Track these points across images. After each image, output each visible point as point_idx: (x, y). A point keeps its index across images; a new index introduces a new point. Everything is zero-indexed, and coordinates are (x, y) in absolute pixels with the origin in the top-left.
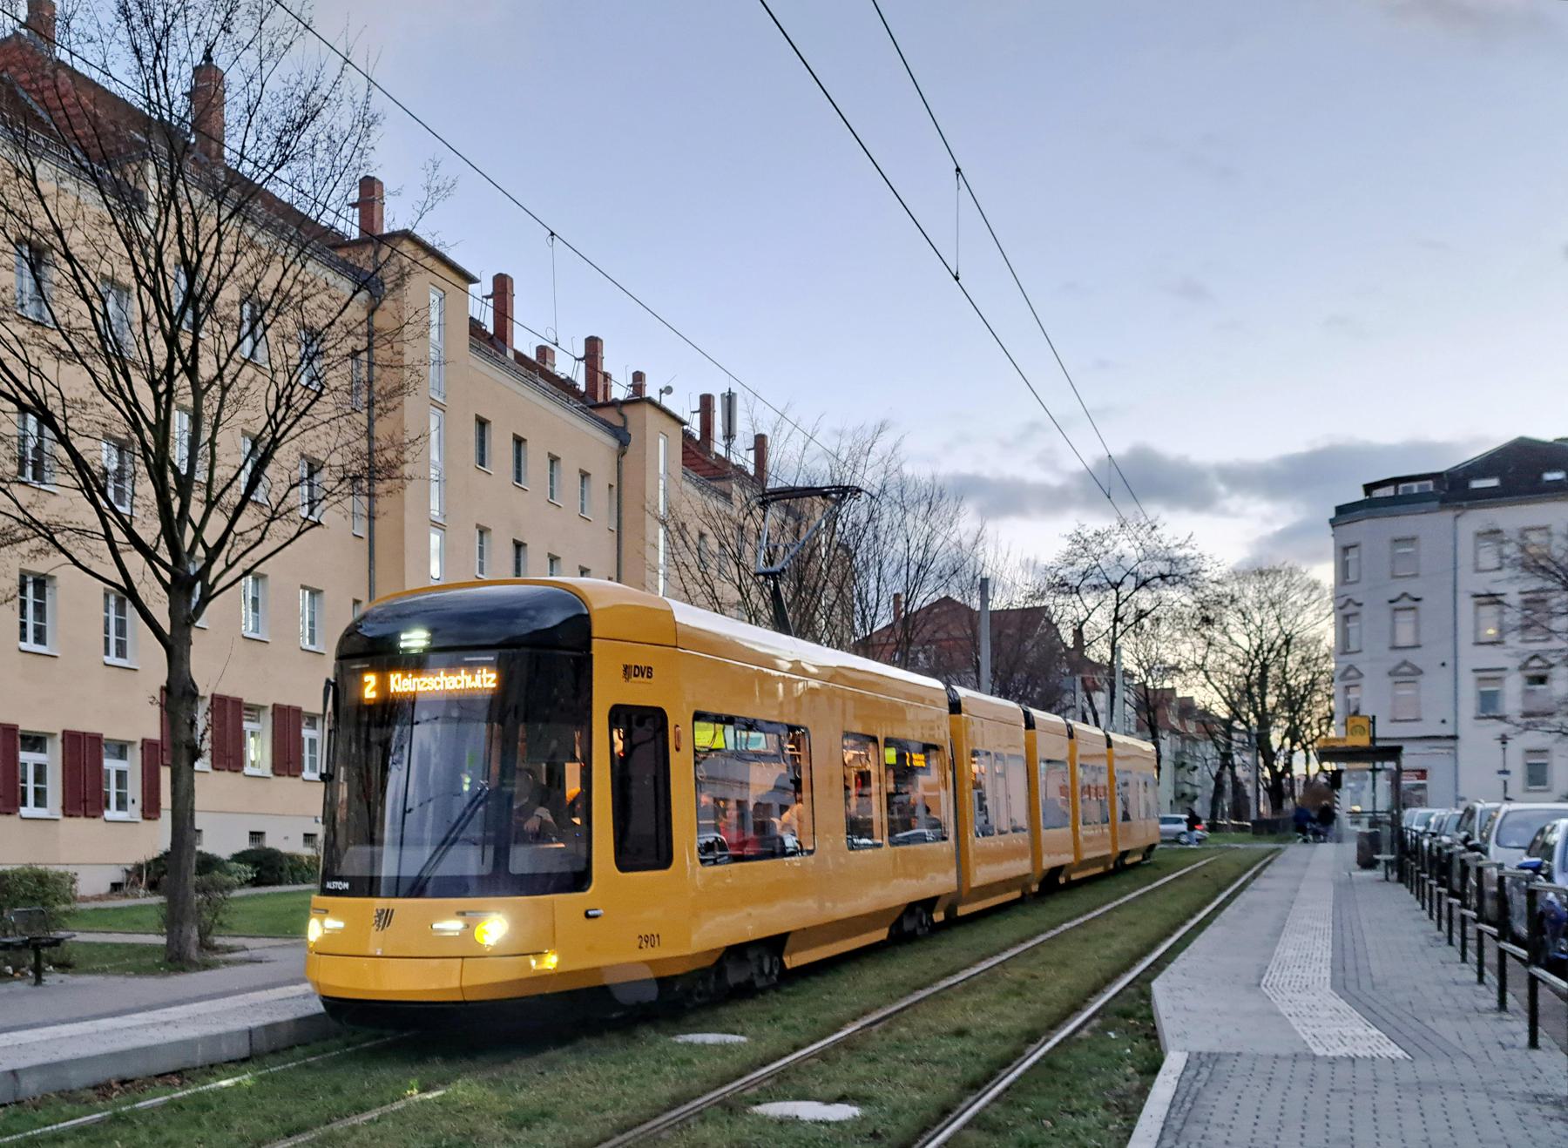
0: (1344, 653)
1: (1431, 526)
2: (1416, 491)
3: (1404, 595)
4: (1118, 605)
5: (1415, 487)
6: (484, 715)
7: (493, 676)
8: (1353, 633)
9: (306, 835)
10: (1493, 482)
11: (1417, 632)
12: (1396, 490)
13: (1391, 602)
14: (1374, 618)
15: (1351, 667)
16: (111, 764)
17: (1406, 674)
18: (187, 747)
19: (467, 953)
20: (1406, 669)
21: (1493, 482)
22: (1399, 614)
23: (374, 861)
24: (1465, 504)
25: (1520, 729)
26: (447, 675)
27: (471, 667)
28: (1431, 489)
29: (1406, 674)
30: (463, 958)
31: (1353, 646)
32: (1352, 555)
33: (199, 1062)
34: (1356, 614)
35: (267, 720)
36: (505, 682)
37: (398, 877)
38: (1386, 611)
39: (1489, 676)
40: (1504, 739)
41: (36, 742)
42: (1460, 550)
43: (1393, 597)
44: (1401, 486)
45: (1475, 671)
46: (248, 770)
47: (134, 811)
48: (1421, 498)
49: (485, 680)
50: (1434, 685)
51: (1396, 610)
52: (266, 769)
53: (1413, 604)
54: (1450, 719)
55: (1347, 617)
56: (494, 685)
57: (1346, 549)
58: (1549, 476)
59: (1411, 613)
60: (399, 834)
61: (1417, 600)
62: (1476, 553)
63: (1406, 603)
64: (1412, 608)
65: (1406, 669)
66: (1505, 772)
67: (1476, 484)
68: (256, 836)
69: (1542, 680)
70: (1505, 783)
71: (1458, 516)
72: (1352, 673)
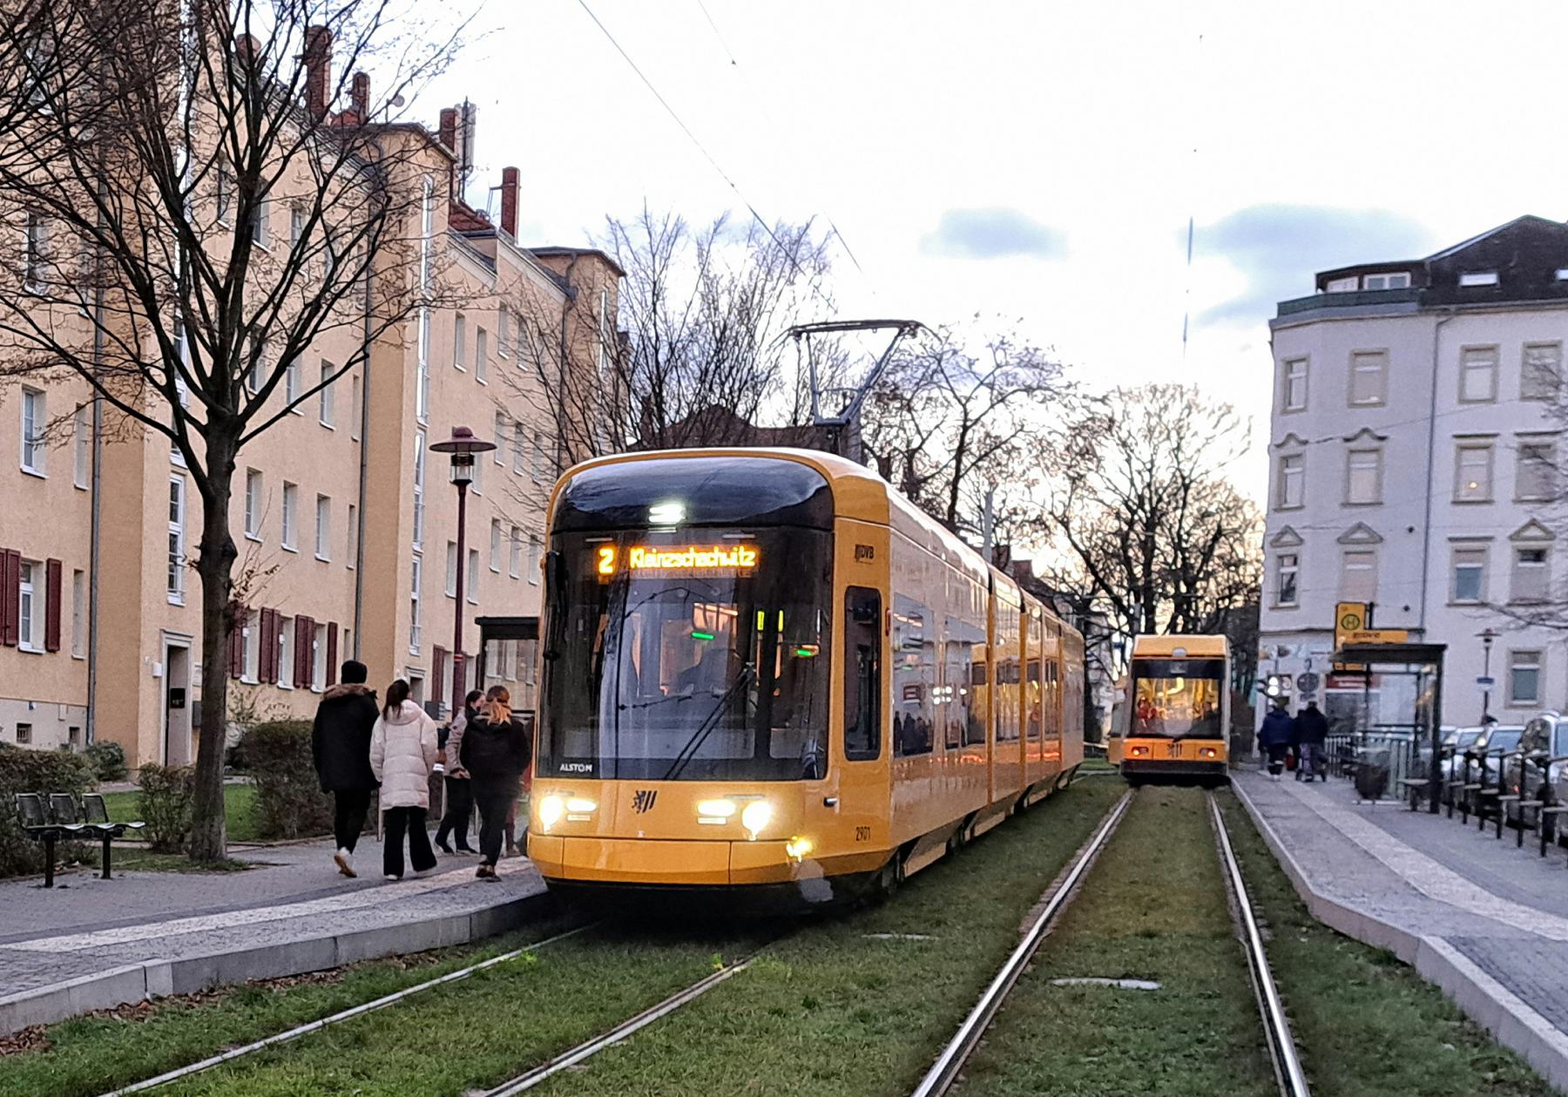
3: (1365, 430)
4: (965, 428)
5: (1387, 281)
6: (633, 592)
7: (752, 554)
10: (1490, 279)
11: (1379, 486)
12: (1360, 285)
13: (1347, 440)
14: (1322, 462)
15: (1287, 530)
17: (1358, 542)
18: (225, 616)
19: (731, 838)
20: (1359, 535)
21: (1490, 279)
22: (1355, 457)
23: (594, 745)
24: (1453, 307)
25: (1522, 623)
26: (697, 551)
27: (728, 544)
28: (1408, 284)
29: (1358, 542)
30: (731, 841)
31: (1292, 501)
32: (1299, 371)
33: (439, 945)
34: (1299, 456)
36: (762, 561)
37: (617, 760)
40: (1488, 636)
43: (1349, 434)
44: (1367, 278)
45: (1451, 540)
49: (744, 558)
50: (1396, 558)
51: (1352, 452)
53: (1376, 444)
55: (1286, 461)
56: (752, 564)
57: (1289, 364)
59: (1373, 456)
60: (865, 709)
61: (1382, 439)
63: (1366, 442)
65: (1359, 535)
66: (1488, 680)
67: (1468, 280)
69: (1538, 555)
70: (1486, 695)
71: (1440, 324)
72: (1288, 538)
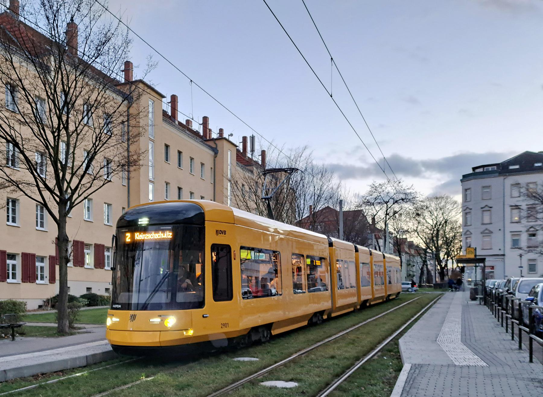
0: (465, 226)
1: (495, 182)
2: (490, 170)
3: (486, 206)
4: (387, 209)
5: (490, 168)
6: (168, 247)
7: (171, 234)
8: (469, 219)
9: (106, 289)
10: (517, 167)
11: (491, 218)
12: (484, 170)
13: (482, 208)
14: (476, 214)
15: (468, 231)
16: (38, 264)
17: (487, 233)
18: (65, 258)
19: (162, 329)
20: (487, 231)
21: (517, 167)
22: (485, 212)
23: (130, 298)
24: (507, 174)
25: (526, 252)
26: (155, 233)
27: (163, 231)
28: (496, 169)
29: (487, 233)
30: (160, 331)
31: (469, 224)
32: (468, 192)
33: (69, 367)
34: (470, 212)
35: (92, 249)
36: (175, 236)
37: (138, 303)
38: (480, 211)
39: (516, 234)
40: (521, 256)
41: (12, 257)
42: (505, 190)
43: (483, 206)
44: (485, 168)
45: (511, 232)
46: (86, 266)
47: (46, 281)
48: (492, 172)
49: (168, 235)
50: (497, 237)
51: (483, 211)
52: (92, 266)
53: (489, 209)
54: (502, 249)
55: (466, 214)
56: (171, 237)
57: (466, 190)
58: (536, 165)
59: (489, 212)
60: (138, 288)
61: (491, 207)
62: (511, 191)
63: (487, 208)
64: (489, 210)
65: (487, 231)
66: (521, 267)
67: (511, 167)
68: (89, 289)
69: (534, 235)
70: (521, 271)
71: (505, 178)
72: (468, 233)
